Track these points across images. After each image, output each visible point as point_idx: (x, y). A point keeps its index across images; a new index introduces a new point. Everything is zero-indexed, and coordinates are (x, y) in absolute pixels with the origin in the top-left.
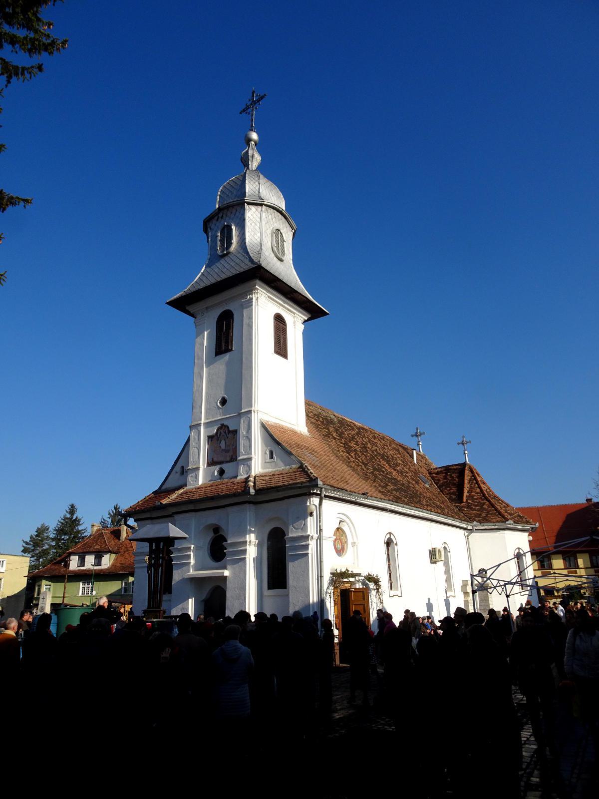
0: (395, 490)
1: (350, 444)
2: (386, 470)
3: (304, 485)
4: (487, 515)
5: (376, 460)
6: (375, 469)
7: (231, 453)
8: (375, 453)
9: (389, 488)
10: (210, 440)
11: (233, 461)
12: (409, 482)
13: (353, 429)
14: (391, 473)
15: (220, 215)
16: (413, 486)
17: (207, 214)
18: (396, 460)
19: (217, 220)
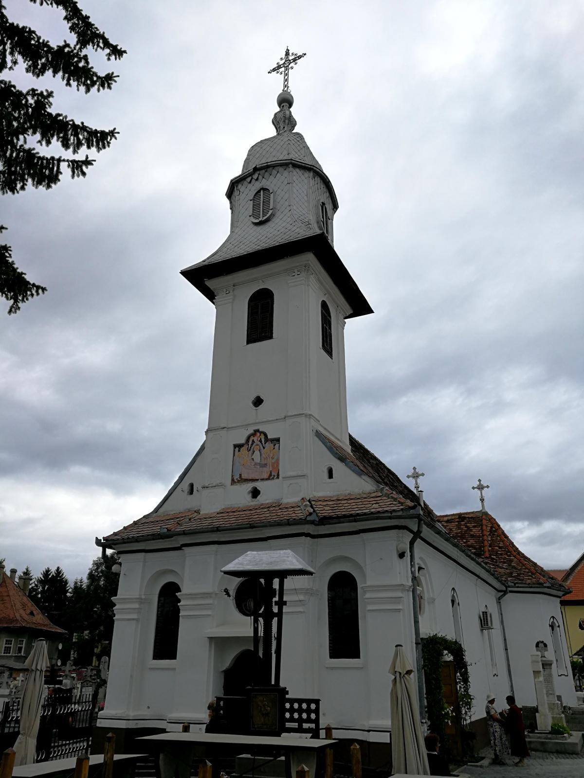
3: (394, 514)
10: (237, 449)
11: (273, 479)
15: (255, 177)
19: (250, 182)
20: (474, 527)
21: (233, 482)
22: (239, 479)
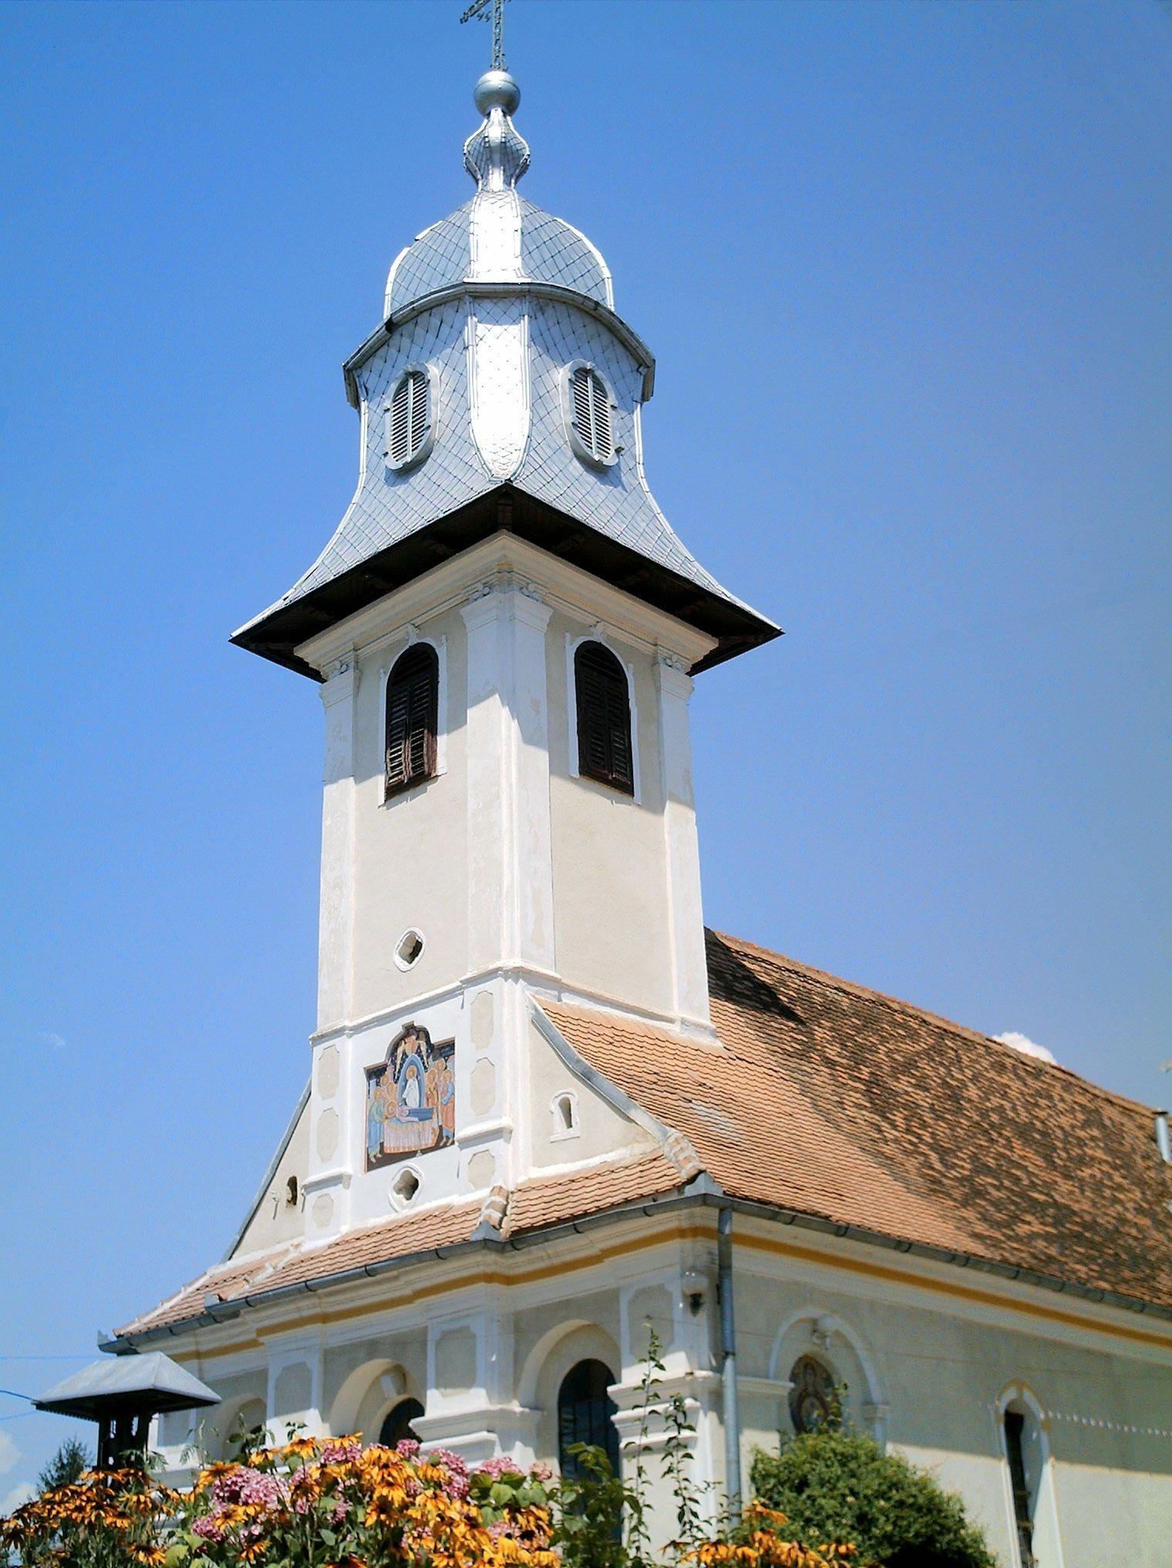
0: (1047, 1237)
1: (892, 1083)
2: (1030, 1174)
7: (434, 1123)
8: (995, 1118)
9: (1022, 1229)
10: (373, 1082)
11: (445, 1146)
12: (1122, 1220)
13: (914, 1036)
14: (1050, 1186)
16: (1140, 1231)
17: (348, 352)
18: (1080, 1147)
21: (371, 1166)
22: (379, 1156)
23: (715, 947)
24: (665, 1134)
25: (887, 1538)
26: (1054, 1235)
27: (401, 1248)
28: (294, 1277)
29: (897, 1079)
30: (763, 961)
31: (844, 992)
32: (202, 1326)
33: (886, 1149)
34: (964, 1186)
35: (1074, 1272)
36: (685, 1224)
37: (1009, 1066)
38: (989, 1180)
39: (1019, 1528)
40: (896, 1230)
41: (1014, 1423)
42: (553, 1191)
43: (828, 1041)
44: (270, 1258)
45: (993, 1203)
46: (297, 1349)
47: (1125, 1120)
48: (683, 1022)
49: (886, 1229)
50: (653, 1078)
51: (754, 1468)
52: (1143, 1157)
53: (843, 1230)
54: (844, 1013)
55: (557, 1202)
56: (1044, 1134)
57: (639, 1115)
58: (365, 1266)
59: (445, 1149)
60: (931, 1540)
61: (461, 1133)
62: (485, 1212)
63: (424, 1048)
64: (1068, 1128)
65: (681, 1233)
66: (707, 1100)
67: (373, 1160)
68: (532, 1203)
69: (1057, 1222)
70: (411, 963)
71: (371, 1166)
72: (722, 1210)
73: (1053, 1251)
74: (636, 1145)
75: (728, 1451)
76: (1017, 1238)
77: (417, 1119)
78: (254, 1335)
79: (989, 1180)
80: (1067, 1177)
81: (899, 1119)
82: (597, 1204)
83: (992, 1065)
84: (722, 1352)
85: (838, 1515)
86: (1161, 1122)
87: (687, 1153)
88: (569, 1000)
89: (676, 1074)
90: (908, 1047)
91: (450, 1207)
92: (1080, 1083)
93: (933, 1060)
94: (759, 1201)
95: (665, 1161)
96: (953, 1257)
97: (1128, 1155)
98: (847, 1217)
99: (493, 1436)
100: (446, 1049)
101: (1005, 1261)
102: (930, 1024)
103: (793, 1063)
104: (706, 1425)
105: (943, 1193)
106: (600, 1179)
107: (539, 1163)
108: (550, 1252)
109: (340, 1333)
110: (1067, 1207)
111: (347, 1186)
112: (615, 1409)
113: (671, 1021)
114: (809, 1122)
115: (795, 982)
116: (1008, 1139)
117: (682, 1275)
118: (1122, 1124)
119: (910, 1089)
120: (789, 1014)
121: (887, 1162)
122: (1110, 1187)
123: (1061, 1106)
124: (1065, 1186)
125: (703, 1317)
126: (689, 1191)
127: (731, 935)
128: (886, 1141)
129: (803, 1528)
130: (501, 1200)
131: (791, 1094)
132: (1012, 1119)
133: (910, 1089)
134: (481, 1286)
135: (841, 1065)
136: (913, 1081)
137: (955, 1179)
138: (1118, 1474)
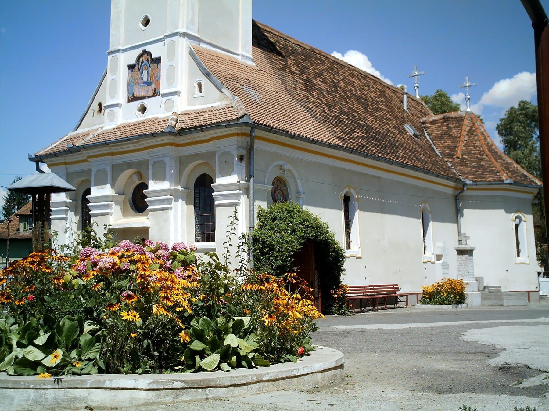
0: (363, 138)
1: (315, 81)
2: (359, 114)
4: (483, 173)
5: (347, 102)
6: (342, 112)
7: (153, 87)
8: (349, 94)
9: (355, 135)
10: (130, 70)
11: (156, 96)
12: (389, 131)
13: (323, 63)
14: (365, 118)
16: (394, 135)
18: (377, 104)
20: (454, 127)
21: (129, 101)
22: (132, 97)
23: (255, 26)
24: (234, 98)
25: (302, 237)
26: (365, 137)
27: (139, 132)
28: (101, 139)
29: (316, 79)
30: (272, 33)
31: (300, 46)
32: (67, 154)
33: (310, 105)
34: (336, 119)
35: (371, 150)
36: (239, 132)
37: (356, 74)
38: (345, 117)
39: (346, 231)
40: (311, 136)
41: (347, 199)
42: (194, 115)
43: (292, 64)
44: (91, 131)
45: (346, 126)
46: (103, 164)
47: (393, 95)
48: (242, 55)
49: (308, 136)
50: (231, 76)
51: (259, 213)
52: (398, 108)
53: (293, 136)
54: (299, 54)
55: (195, 120)
56: (365, 100)
57: (225, 91)
58: (127, 137)
59: (156, 97)
60: (317, 237)
61: (162, 92)
62: (170, 121)
63: (149, 59)
64: (374, 98)
65: (238, 134)
66: (249, 85)
67: (130, 99)
68: (187, 119)
69: (367, 132)
70: (146, 27)
71: (129, 101)
72: (251, 128)
73: (365, 143)
74: (223, 101)
75: (250, 208)
76: (353, 138)
77: (146, 85)
78: (86, 158)
79: (345, 117)
80: (371, 115)
81: (315, 94)
82: (209, 122)
83: (350, 74)
84: (250, 176)
85: (286, 230)
86: (405, 96)
87: (241, 107)
88: (203, 45)
89: (239, 75)
90: (321, 67)
91: (157, 118)
92: (379, 81)
93: (329, 72)
94: (265, 125)
95: (233, 108)
96: (330, 146)
97: (393, 107)
98: (295, 131)
99: (172, 197)
100: (158, 61)
101: (348, 147)
102: (329, 59)
103: (279, 72)
104: (243, 199)
105: (328, 122)
106: (210, 113)
107: (189, 104)
108: (192, 137)
109: (118, 159)
110: (371, 126)
111: (120, 108)
112: (213, 191)
113: (238, 55)
114: (284, 95)
115: (282, 42)
116: (352, 102)
117: (237, 149)
118: (392, 96)
119: (320, 83)
120: (279, 54)
121: (309, 110)
122: (385, 119)
123: (372, 89)
124: (370, 119)
125: (244, 163)
126: (241, 121)
127: (261, 22)
128: (310, 102)
129: (274, 233)
130: (175, 117)
131: (278, 84)
132: (355, 95)
133: (320, 83)
134: (168, 147)
135: (297, 74)
136: (321, 80)
137: (333, 116)
138: (379, 215)
